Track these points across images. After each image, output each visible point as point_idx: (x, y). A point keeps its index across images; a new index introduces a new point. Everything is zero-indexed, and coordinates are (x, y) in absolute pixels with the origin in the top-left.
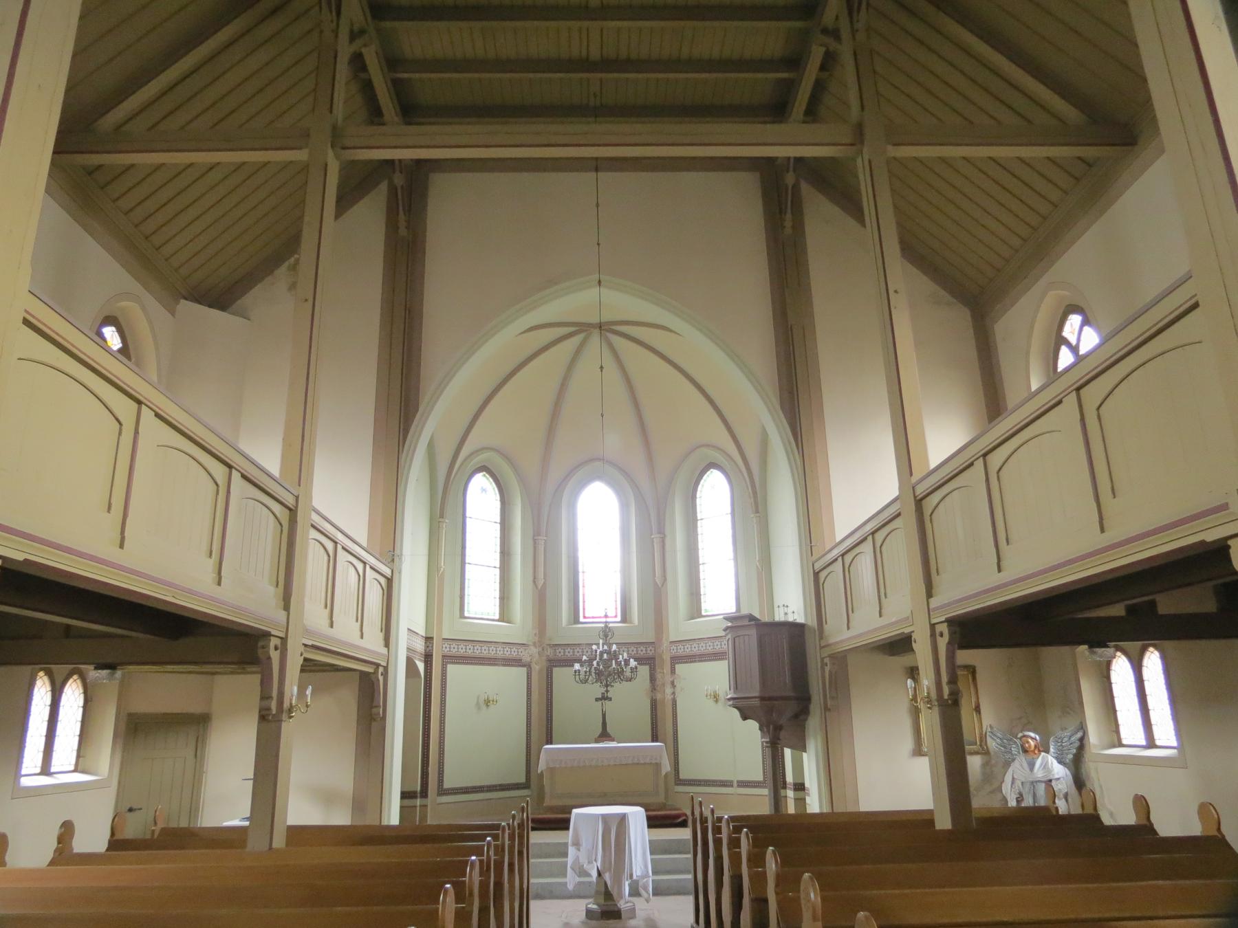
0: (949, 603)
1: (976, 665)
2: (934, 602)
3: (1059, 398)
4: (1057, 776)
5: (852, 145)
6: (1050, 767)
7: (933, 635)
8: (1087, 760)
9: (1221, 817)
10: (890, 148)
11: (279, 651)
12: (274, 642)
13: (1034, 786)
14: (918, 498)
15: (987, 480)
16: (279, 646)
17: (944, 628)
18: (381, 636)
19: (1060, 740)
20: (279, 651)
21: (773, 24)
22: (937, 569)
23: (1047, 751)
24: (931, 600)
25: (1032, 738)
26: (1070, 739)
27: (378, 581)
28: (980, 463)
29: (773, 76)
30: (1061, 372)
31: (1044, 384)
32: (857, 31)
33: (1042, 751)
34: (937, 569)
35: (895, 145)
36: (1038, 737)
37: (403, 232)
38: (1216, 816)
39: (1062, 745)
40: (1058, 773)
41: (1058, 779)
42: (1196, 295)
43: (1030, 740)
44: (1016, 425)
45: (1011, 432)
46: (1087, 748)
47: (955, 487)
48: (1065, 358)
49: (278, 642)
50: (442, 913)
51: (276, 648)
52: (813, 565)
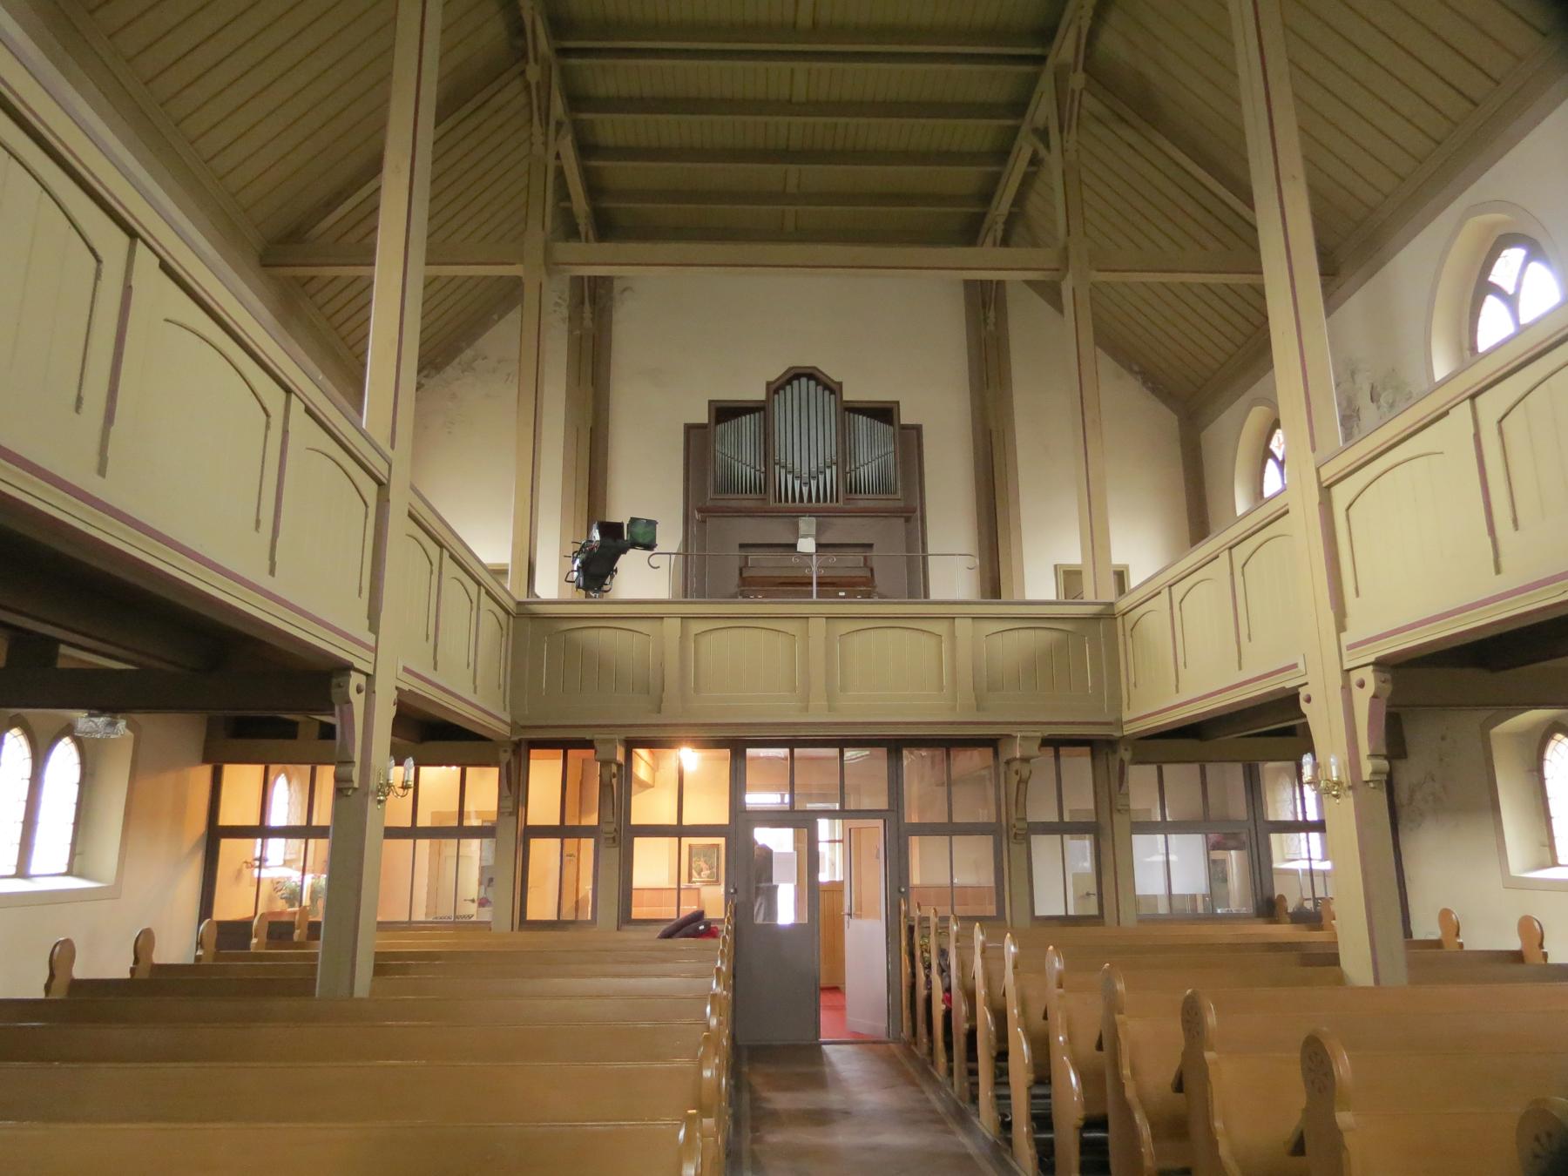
2: (1348, 638)
3: (1216, 553)
5: (1057, 270)
7: (1346, 687)
9: (1544, 930)
10: (1094, 273)
11: (363, 694)
12: (356, 680)
14: (1324, 485)
15: (1232, 574)
17: (1368, 675)
18: (363, 604)
20: (363, 694)
21: (985, 122)
22: (1185, 663)
24: (1343, 635)
27: (459, 580)
28: (1225, 556)
29: (995, 122)
30: (1438, 382)
31: (1453, 372)
32: (1067, 151)
34: (1185, 663)
35: (1099, 270)
37: (588, 323)
38: (1539, 930)
40: (479, 814)
42: (1287, 504)
44: (1372, 451)
45: (1266, 521)
47: (1269, 537)
48: (1494, 325)
49: (362, 680)
51: (359, 690)
52: (1318, 470)
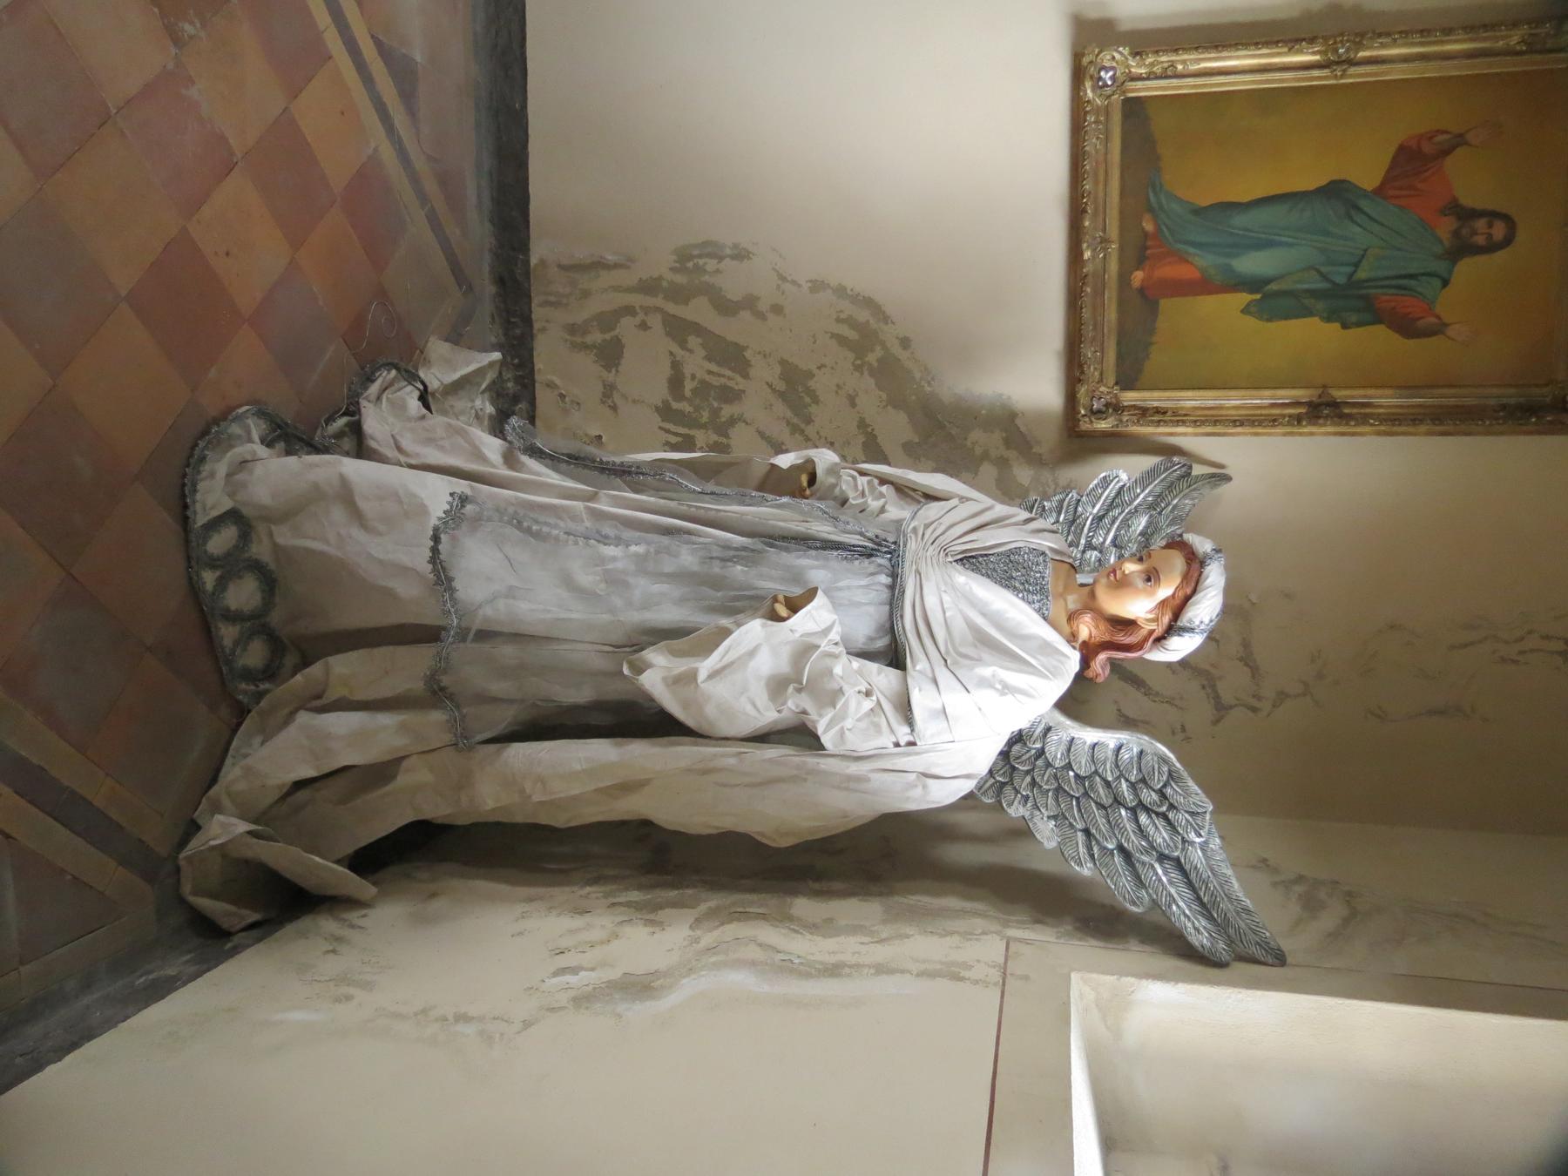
0: (594, 471)
1: (1342, 331)
4: (921, 700)
6: (986, 671)
8: (1013, 932)
13: (868, 554)
16: (1206, 683)
19: (1149, 797)
23: (1074, 703)
25: (1177, 608)
26: (1162, 858)
33: (1085, 662)
36: (1180, 648)
39: (1118, 801)
41: (905, 709)
43: (1165, 591)
46: (1090, 949)
50: (1287, 399)
